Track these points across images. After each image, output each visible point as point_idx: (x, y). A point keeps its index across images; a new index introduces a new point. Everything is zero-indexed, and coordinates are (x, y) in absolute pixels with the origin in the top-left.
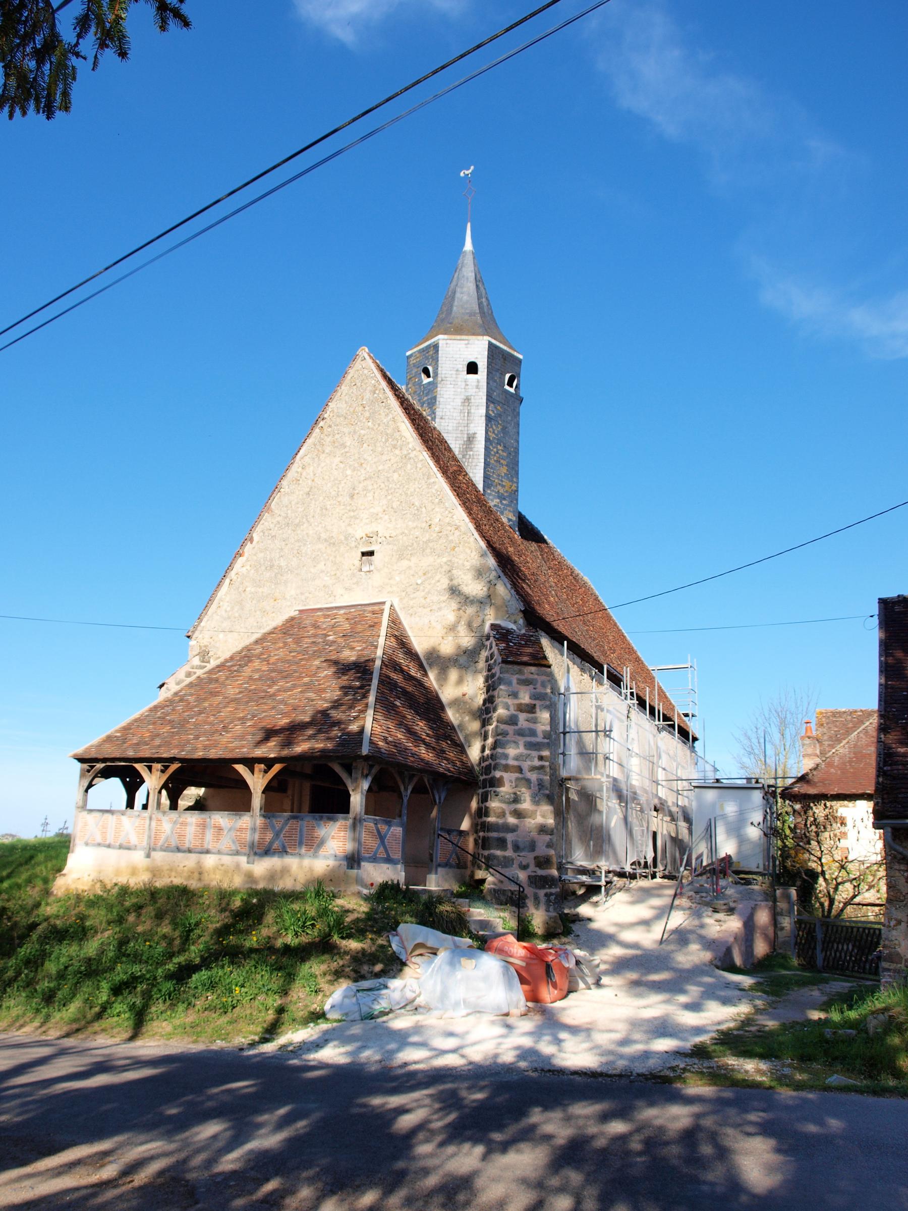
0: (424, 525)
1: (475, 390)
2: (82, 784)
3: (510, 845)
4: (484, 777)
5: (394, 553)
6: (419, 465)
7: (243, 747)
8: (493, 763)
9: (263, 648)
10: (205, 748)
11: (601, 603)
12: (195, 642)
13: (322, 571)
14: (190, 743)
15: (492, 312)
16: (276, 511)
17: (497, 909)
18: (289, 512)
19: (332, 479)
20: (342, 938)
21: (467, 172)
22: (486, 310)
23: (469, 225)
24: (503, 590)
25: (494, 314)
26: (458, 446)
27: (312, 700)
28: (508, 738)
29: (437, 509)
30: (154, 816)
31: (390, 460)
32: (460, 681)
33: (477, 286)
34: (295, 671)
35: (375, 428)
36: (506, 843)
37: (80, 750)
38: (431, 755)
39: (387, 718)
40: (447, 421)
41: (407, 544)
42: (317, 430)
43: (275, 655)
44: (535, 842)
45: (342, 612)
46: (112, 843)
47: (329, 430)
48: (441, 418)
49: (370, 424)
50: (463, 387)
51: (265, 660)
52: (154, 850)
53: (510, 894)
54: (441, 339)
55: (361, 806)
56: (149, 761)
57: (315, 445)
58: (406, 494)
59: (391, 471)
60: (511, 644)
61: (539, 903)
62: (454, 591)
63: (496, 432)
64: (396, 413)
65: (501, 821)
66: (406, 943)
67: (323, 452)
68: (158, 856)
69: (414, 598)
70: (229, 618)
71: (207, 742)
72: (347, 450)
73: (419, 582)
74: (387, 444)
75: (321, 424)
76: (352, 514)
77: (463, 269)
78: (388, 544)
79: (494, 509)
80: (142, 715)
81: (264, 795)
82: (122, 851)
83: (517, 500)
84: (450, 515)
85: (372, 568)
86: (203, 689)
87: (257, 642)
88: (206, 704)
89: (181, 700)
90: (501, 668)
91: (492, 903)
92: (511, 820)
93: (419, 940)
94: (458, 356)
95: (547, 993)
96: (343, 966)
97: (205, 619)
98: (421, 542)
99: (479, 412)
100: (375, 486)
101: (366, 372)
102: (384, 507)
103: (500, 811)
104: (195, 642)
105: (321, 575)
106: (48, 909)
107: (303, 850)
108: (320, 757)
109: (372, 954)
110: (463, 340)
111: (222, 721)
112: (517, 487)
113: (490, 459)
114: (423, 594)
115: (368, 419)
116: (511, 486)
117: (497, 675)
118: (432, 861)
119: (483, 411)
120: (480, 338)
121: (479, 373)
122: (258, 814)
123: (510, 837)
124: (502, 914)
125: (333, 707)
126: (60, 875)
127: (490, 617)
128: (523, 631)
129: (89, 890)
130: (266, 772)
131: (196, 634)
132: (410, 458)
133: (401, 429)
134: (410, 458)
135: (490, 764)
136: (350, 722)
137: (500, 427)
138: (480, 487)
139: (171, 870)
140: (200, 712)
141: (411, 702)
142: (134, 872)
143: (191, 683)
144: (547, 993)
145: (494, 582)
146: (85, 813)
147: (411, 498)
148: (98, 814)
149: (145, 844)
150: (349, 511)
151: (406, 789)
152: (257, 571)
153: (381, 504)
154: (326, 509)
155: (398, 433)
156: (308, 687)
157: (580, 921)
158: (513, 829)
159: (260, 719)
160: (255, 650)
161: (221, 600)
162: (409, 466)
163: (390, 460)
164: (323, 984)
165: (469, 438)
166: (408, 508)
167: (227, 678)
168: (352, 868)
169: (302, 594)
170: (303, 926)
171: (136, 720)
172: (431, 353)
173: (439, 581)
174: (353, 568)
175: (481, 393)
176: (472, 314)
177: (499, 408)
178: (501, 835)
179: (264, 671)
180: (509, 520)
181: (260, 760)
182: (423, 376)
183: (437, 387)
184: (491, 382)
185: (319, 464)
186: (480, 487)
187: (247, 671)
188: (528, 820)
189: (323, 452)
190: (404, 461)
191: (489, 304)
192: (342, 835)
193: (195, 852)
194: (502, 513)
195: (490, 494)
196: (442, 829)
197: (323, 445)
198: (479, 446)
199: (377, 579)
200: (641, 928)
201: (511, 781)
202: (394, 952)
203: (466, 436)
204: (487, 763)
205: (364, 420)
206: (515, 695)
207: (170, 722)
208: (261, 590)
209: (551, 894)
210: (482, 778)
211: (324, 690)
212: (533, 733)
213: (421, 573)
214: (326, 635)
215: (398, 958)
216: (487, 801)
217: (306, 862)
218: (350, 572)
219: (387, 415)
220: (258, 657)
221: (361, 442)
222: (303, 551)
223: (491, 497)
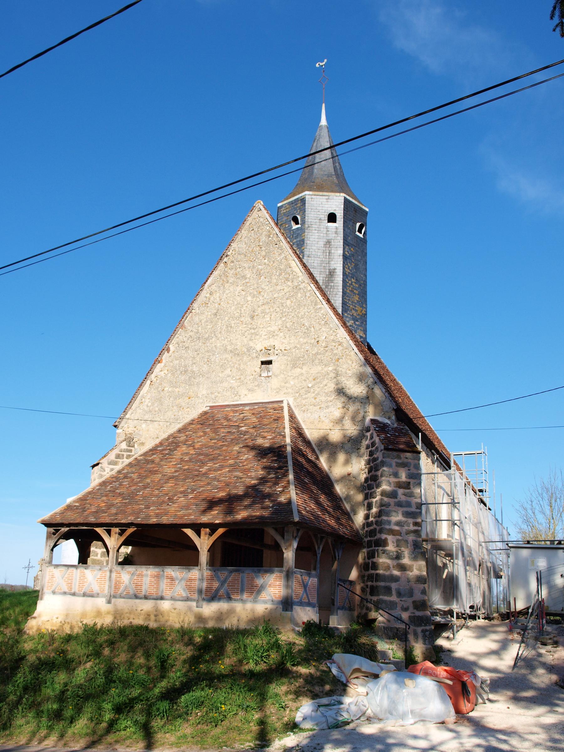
0: (313, 341)
1: (334, 235)
2: (48, 544)
3: (394, 592)
4: (369, 539)
5: (289, 363)
6: (308, 295)
7: (190, 515)
8: (378, 528)
9: (187, 436)
10: (157, 515)
12: (121, 430)
13: (229, 376)
14: (143, 512)
15: (343, 174)
16: (189, 328)
17: (386, 642)
18: (200, 328)
19: (236, 303)
20: (293, 665)
21: (321, 64)
22: (339, 172)
23: (324, 105)
24: (378, 392)
25: (345, 175)
26: (321, 278)
27: (241, 478)
28: (390, 508)
29: (323, 329)
30: (113, 570)
31: (283, 290)
32: (347, 462)
34: (220, 455)
35: (270, 264)
36: (391, 590)
37: (46, 516)
38: (333, 521)
39: (303, 493)
40: (313, 259)
41: (299, 355)
42: (222, 265)
43: (198, 442)
44: (413, 589)
45: (247, 408)
46: (77, 591)
48: (308, 257)
49: (266, 261)
50: (325, 232)
51: (190, 446)
52: (115, 597)
53: (395, 631)
55: (293, 561)
56: (108, 527)
57: (220, 276)
58: (298, 317)
59: (284, 299)
60: (388, 435)
61: (417, 637)
62: (341, 392)
63: (350, 268)
64: (288, 253)
65: (387, 573)
66: (343, 669)
67: (228, 282)
68: (121, 603)
69: (306, 398)
70: (150, 411)
71: (157, 511)
72: (247, 280)
73: (310, 385)
74: (281, 277)
75: (225, 260)
76: (253, 331)
77: (321, 139)
78: (284, 355)
80: (94, 489)
81: (209, 553)
82: (85, 598)
83: (366, 321)
84: (334, 334)
85: (270, 374)
86: (142, 468)
87: (179, 431)
88: (148, 480)
89: (126, 477)
90: (383, 454)
91: (383, 638)
92: (396, 573)
93: (356, 666)
94: (321, 208)
95: (465, 706)
96: (299, 687)
97: (130, 412)
98: (311, 354)
100: (272, 310)
101: (262, 220)
102: (279, 327)
103: (386, 565)
104: (121, 430)
105: (228, 379)
106: (26, 645)
107: (245, 596)
108: (259, 523)
109: (318, 678)
110: (324, 196)
111: (167, 494)
112: (366, 312)
113: (347, 289)
114: (313, 395)
115: (264, 257)
117: (380, 460)
118: (334, 605)
119: (341, 251)
120: (338, 194)
121: (337, 222)
122: (205, 568)
123: (394, 586)
124: (391, 647)
125: (259, 484)
126: (32, 618)
127: (371, 414)
128: (396, 425)
129: (58, 630)
130: (211, 535)
133: (292, 265)
135: (375, 529)
136: (278, 496)
137: (353, 264)
139: (130, 613)
140: (145, 487)
141: (315, 481)
142: (99, 613)
143: (130, 463)
144: (465, 706)
145: (372, 386)
146: (52, 568)
147: (302, 320)
148: (63, 569)
149: (106, 591)
150: (251, 329)
151: (319, 548)
152: (173, 374)
153: (277, 324)
154: (231, 327)
155: (290, 269)
156: (234, 468)
157: (442, 652)
158: (395, 579)
159: (199, 492)
160: (180, 437)
161: (143, 397)
162: (299, 295)
163: (283, 290)
164: (288, 700)
165: (330, 272)
166: (299, 328)
167: (161, 460)
168: (287, 610)
169: (212, 393)
170: (262, 657)
171: (90, 493)
172: (299, 205)
173: (326, 385)
174: (254, 374)
175: (339, 238)
176: (329, 175)
177: (352, 249)
178: (388, 584)
179: (192, 454)
181: (205, 525)
183: (304, 232)
185: (224, 292)
187: (178, 454)
188: (408, 572)
189: (228, 282)
190: (295, 291)
191: (341, 168)
192: (277, 584)
193: (150, 599)
195: (347, 317)
196: (340, 580)
197: (227, 276)
198: (338, 279)
199: (275, 382)
200: (494, 657)
201: (393, 542)
202: (334, 676)
203: (328, 271)
204: (372, 528)
205: (261, 258)
206: (396, 475)
207: (120, 494)
208: (177, 390)
209: (426, 630)
210: (366, 540)
211: (249, 470)
212: (409, 504)
213: (311, 379)
214: (238, 427)
215: (339, 681)
216: (374, 557)
217: (249, 606)
218: (252, 377)
219: (280, 254)
220: (185, 443)
221: (259, 275)
222: (213, 360)
223: (347, 319)
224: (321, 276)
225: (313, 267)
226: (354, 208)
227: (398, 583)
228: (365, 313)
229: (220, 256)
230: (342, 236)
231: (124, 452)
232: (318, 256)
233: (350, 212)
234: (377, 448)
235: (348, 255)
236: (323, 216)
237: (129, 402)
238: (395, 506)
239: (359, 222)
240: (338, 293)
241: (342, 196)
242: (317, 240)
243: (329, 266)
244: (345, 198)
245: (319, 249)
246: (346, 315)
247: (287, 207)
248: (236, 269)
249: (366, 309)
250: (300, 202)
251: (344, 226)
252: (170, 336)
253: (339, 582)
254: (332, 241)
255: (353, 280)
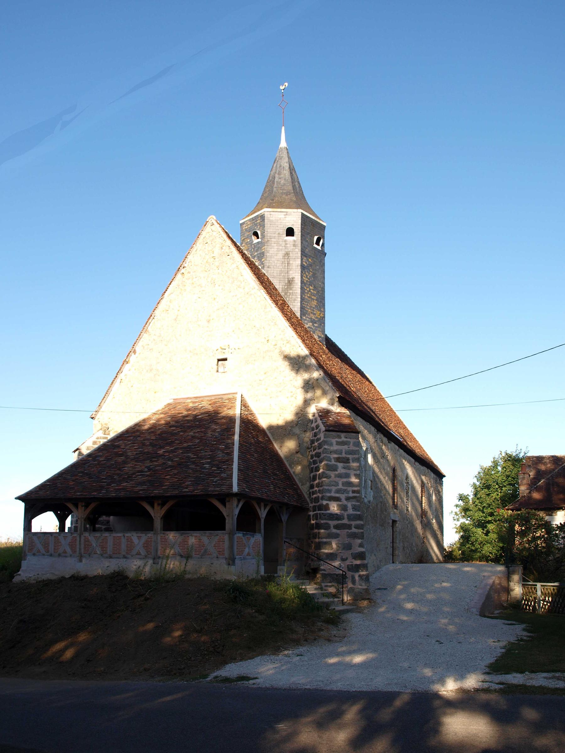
4: (314, 504)
8: (320, 495)
11: (378, 391)
23: (283, 128)
31: (236, 296)
33: (291, 173)
47: (189, 275)
48: (268, 267)
50: (283, 245)
54: (266, 211)
63: (308, 277)
75: (183, 271)
79: (309, 329)
83: (324, 323)
90: (325, 434)
99: (296, 263)
112: (324, 315)
113: (305, 296)
116: (320, 314)
119: (299, 262)
120: (295, 210)
131: (99, 415)
132: (251, 295)
134: (251, 295)
138: (298, 314)
165: (289, 281)
175: (297, 250)
177: (310, 260)
180: (319, 337)
182: (254, 238)
184: (304, 242)
186: (298, 314)
191: (300, 186)
194: (314, 332)
195: (305, 320)
198: (296, 287)
203: (287, 279)
223: (306, 322)
224: (281, 284)
225: (272, 276)
226: (312, 223)
227: (338, 539)
228: (323, 316)
229: (178, 268)
230: (300, 248)
231: (100, 439)
232: (278, 267)
233: (308, 227)
234: (320, 430)
235: (306, 265)
236: (282, 231)
237: (103, 397)
238: (335, 477)
239: (317, 236)
240: (296, 299)
241: (299, 212)
242: (276, 252)
243: (288, 276)
244: (302, 214)
245: (278, 261)
246: (304, 318)
247: (249, 223)
248: (192, 279)
249: (325, 313)
250: (259, 218)
251: (301, 239)
252: (136, 340)
253: (285, 540)
254: (291, 253)
255: (311, 287)
